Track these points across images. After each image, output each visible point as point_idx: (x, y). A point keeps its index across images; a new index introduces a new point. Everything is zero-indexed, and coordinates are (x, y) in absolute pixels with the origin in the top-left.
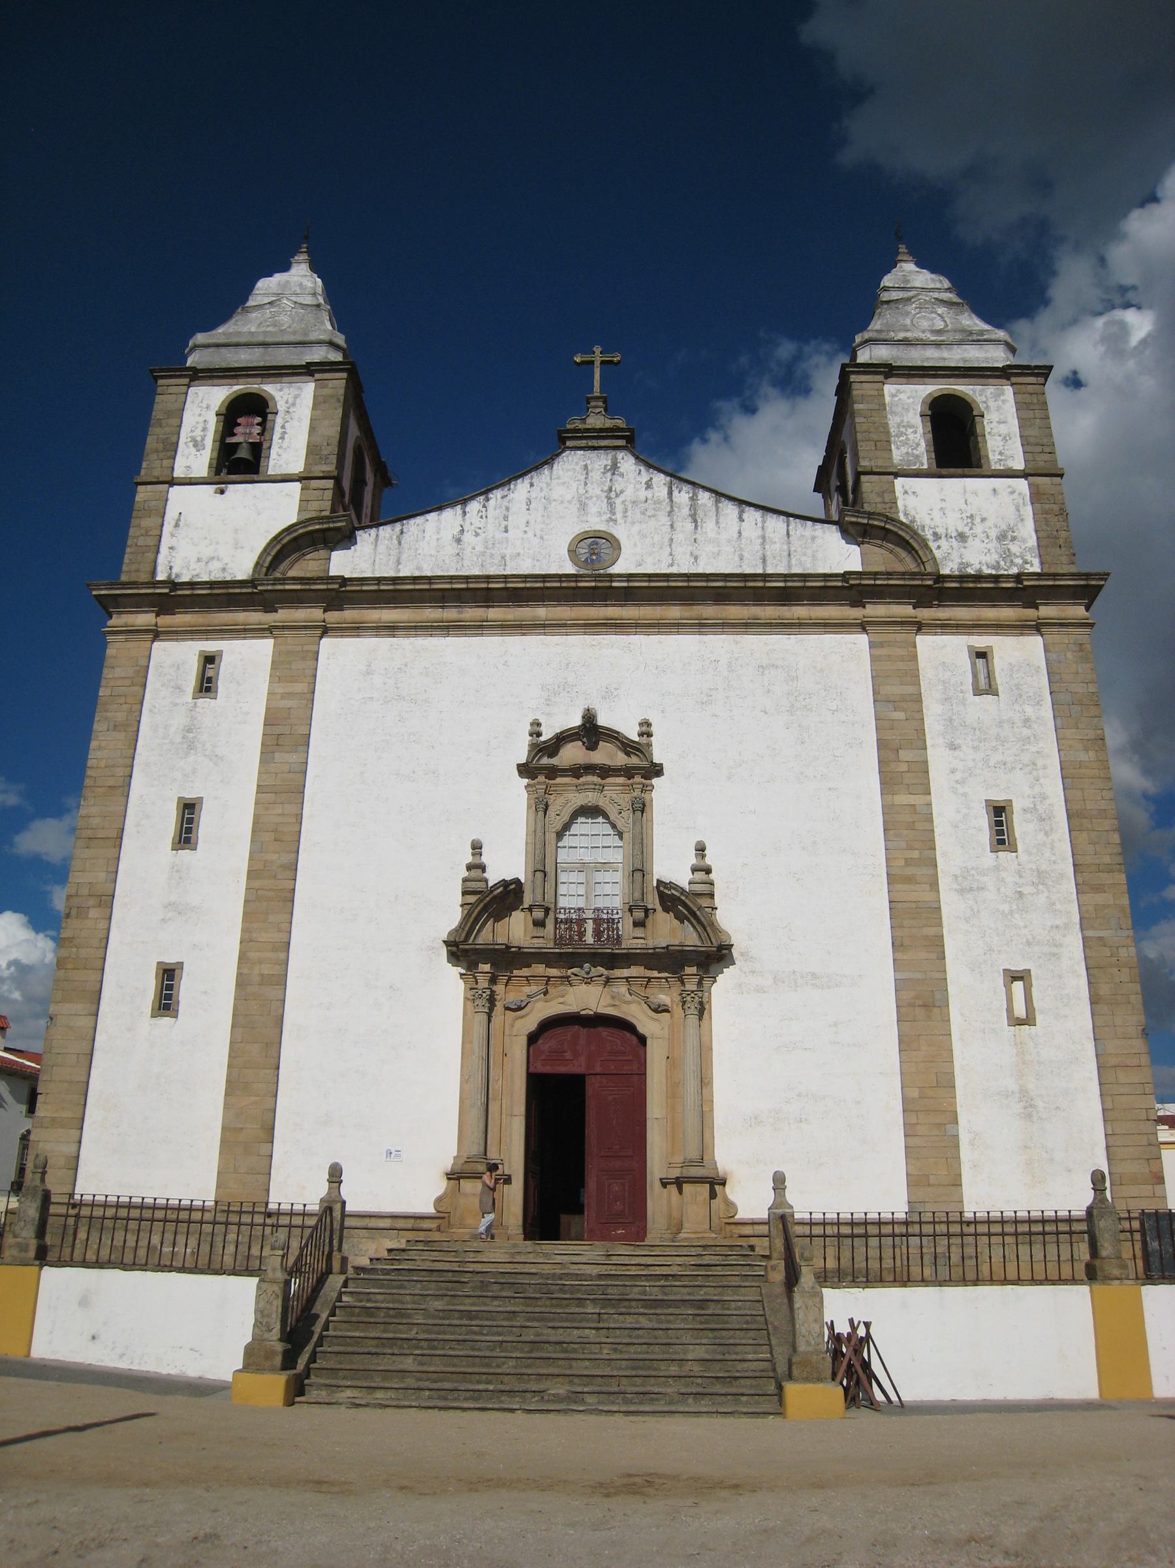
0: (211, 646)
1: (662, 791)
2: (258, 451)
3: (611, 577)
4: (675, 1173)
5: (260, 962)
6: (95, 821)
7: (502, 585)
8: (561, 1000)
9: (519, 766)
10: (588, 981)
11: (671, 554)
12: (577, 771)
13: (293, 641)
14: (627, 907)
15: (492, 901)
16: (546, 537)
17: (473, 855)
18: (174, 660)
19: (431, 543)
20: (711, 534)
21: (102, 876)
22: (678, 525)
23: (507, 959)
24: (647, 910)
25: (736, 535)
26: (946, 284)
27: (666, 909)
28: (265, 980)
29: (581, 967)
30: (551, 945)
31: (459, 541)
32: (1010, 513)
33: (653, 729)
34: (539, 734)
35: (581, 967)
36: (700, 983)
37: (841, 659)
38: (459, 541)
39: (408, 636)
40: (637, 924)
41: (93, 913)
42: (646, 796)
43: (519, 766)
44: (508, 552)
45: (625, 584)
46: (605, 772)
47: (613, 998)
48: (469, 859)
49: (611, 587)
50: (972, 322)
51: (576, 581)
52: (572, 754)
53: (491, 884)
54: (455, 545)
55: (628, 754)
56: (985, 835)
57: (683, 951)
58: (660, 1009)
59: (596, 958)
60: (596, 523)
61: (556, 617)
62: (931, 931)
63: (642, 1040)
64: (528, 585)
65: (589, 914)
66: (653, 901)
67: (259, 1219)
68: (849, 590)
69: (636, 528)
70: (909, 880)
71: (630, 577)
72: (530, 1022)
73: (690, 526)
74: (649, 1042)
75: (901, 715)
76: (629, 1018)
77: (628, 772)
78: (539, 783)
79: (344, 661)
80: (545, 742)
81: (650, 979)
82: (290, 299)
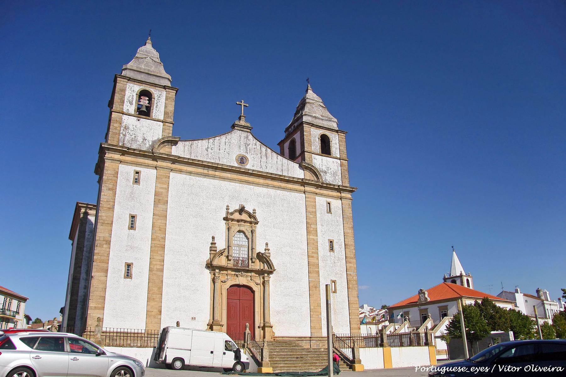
0: (138, 169)
1: (259, 229)
2: (149, 108)
5: (156, 265)
6: (104, 218)
12: (238, 221)
13: (162, 172)
18: (126, 171)
19: (199, 149)
21: (107, 235)
22: (263, 157)
26: (321, 101)
28: (158, 270)
31: (207, 150)
32: (337, 169)
37: (296, 199)
38: (207, 150)
41: (105, 246)
50: (328, 114)
52: (237, 216)
55: (250, 218)
56: (328, 248)
60: (243, 152)
62: (317, 270)
66: (226, 253)
67: (132, 335)
68: (303, 183)
69: (252, 156)
70: (312, 257)
73: (265, 158)
75: (312, 216)
79: (177, 180)
82: (148, 56)
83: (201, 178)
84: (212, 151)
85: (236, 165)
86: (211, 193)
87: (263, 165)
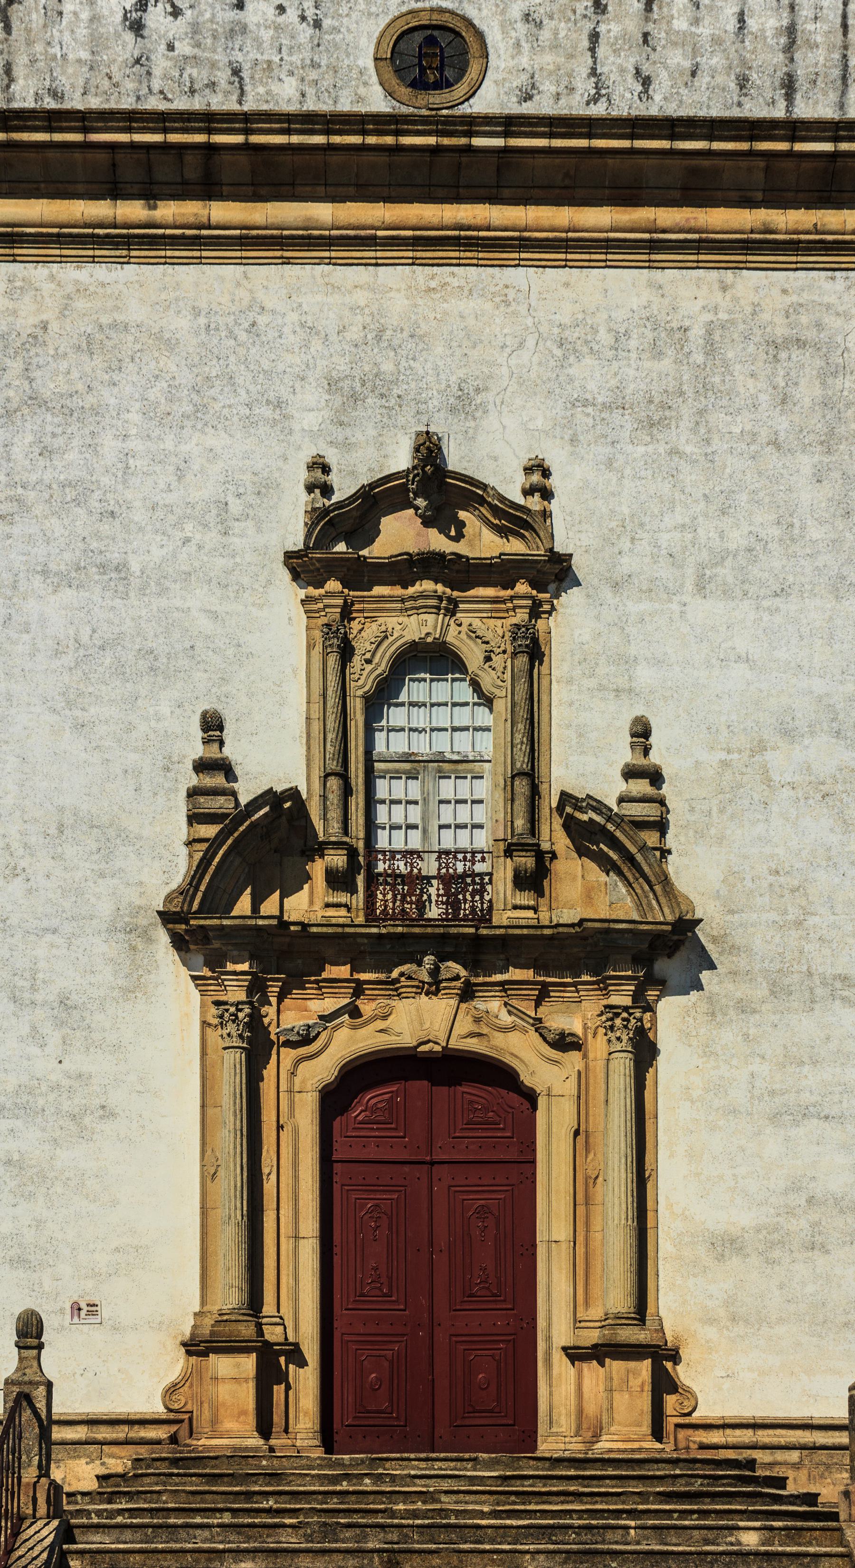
1: (571, 624)
3: (473, 124)
4: (591, 1337)
7: (239, 139)
8: (380, 1024)
9: (289, 556)
10: (434, 987)
11: (593, 72)
12: (408, 568)
14: (502, 846)
15: (252, 840)
16: (327, 23)
17: (206, 742)
20: (681, 24)
23: (289, 957)
24: (540, 855)
25: (732, 25)
27: (582, 852)
29: (420, 964)
30: (361, 919)
31: (137, 27)
33: (555, 482)
34: (327, 490)
35: (420, 964)
36: (638, 996)
38: (137, 27)
39: (45, 260)
40: (521, 881)
42: (541, 624)
43: (289, 556)
44: (246, 56)
45: (499, 142)
46: (461, 573)
47: (477, 1020)
48: (198, 750)
49: (469, 149)
51: (397, 133)
52: (400, 533)
53: (244, 800)
54: (129, 37)
55: (502, 532)
57: (608, 931)
58: (565, 1043)
59: (445, 946)
61: (353, 220)
63: (531, 1097)
64: (295, 139)
65: (430, 866)
66: (554, 836)
71: (510, 124)
72: (323, 1069)
74: (542, 1102)
76: (508, 1060)
77: (502, 572)
78: (330, 595)
80: (340, 505)
81: (545, 985)
83: (100, 272)
84: (179, 27)
85: (377, 101)
86: (186, 378)
87: (617, 64)
